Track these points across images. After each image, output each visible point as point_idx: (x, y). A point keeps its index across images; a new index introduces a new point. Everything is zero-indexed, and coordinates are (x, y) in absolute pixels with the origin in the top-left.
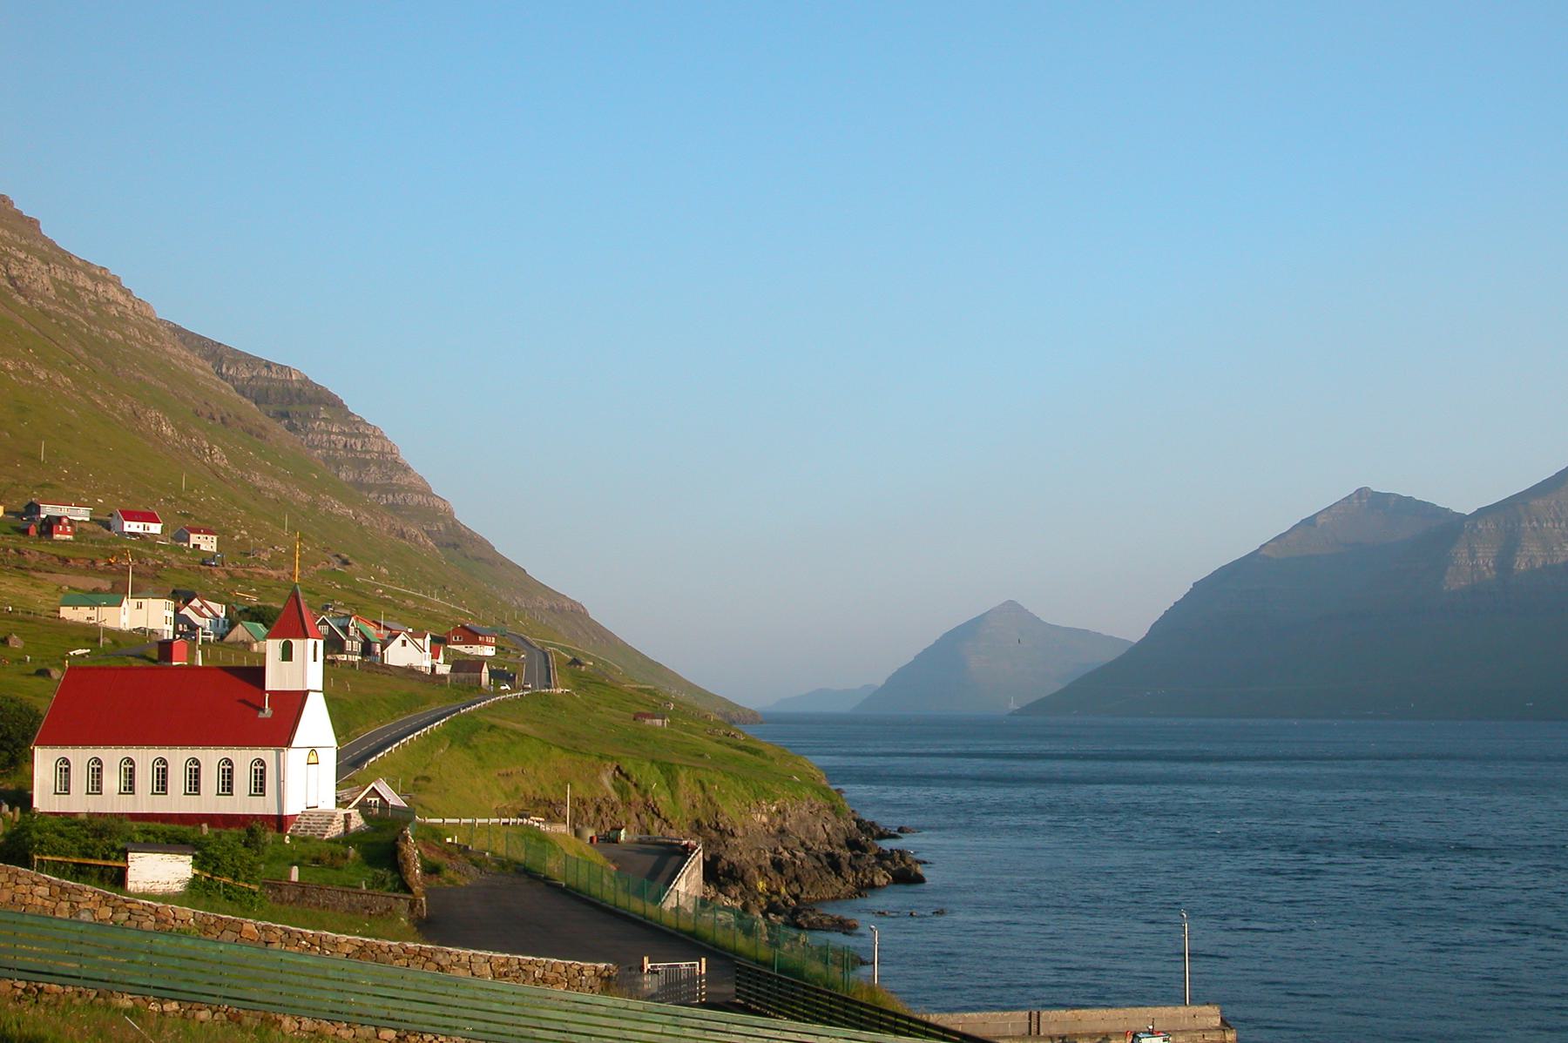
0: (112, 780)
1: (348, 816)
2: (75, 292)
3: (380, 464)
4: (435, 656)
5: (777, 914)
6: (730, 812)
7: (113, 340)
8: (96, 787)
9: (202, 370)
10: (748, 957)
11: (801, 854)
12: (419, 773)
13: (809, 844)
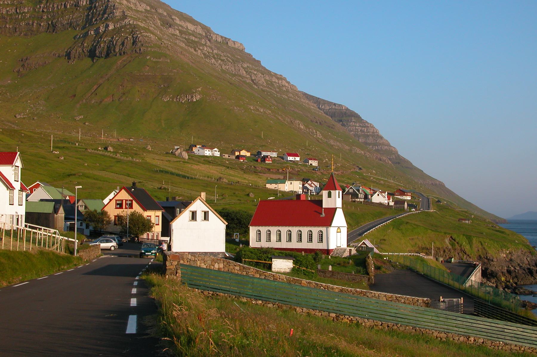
0: (274, 237)
1: (350, 250)
2: (272, 84)
3: (373, 136)
4: (389, 199)
5: (508, 289)
6: (492, 253)
7: (284, 98)
8: (269, 239)
9: (313, 107)
10: (483, 299)
11: (518, 268)
12: (382, 238)
13: (521, 265)
